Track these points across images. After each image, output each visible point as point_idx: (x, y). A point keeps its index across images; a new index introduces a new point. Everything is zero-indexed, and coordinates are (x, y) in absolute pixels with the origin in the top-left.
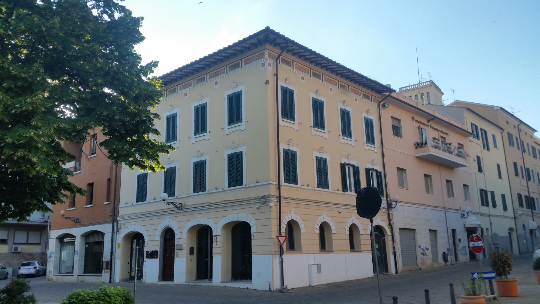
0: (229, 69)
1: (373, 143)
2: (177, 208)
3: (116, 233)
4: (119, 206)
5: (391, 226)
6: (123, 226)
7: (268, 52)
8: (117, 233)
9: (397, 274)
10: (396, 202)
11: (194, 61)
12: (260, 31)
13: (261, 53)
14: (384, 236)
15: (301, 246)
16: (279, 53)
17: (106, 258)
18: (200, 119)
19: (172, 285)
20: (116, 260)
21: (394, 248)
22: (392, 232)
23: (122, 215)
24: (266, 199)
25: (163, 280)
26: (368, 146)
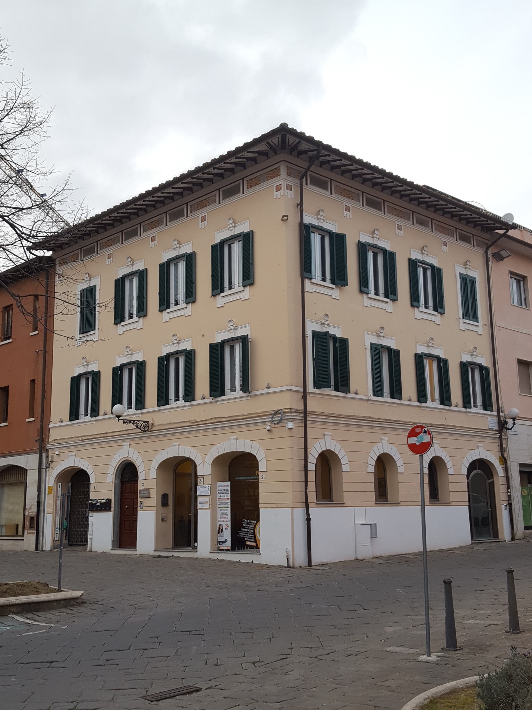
0: (223, 195)
1: (475, 318)
2: (140, 429)
3: (45, 469)
4: (50, 426)
5: (504, 460)
6: (56, 458)
7: (287, 166)
8: (47, 469)
9: (513, 542)
10: (514, 419)
11: (106, 211)
12: (272, 131)
13: (275, 169)
14: (493, 477)
15: (343, 496)
16: (306, 168)
17: (30, 511)
18: (193, 275)
19: (133, 555)
20: (46, 513)
21: (509, 497)
22: (506, 470)
23: (55, 440)
24: (282, 416)
25: (120, 547)
26: (464, 324)
